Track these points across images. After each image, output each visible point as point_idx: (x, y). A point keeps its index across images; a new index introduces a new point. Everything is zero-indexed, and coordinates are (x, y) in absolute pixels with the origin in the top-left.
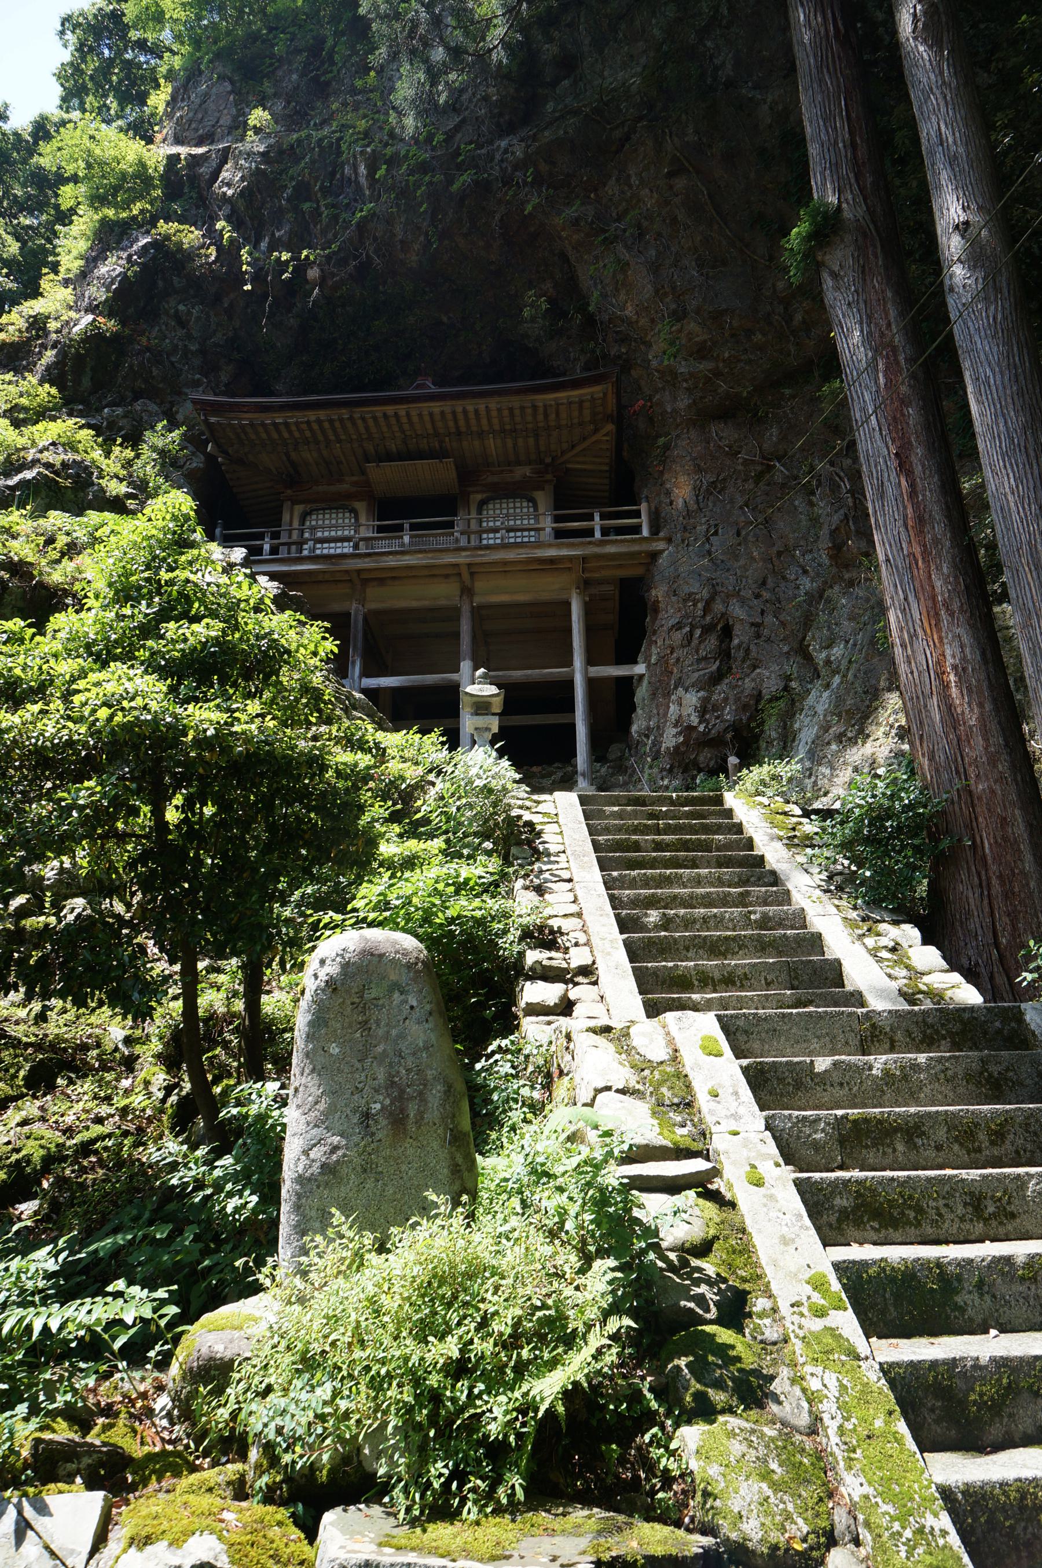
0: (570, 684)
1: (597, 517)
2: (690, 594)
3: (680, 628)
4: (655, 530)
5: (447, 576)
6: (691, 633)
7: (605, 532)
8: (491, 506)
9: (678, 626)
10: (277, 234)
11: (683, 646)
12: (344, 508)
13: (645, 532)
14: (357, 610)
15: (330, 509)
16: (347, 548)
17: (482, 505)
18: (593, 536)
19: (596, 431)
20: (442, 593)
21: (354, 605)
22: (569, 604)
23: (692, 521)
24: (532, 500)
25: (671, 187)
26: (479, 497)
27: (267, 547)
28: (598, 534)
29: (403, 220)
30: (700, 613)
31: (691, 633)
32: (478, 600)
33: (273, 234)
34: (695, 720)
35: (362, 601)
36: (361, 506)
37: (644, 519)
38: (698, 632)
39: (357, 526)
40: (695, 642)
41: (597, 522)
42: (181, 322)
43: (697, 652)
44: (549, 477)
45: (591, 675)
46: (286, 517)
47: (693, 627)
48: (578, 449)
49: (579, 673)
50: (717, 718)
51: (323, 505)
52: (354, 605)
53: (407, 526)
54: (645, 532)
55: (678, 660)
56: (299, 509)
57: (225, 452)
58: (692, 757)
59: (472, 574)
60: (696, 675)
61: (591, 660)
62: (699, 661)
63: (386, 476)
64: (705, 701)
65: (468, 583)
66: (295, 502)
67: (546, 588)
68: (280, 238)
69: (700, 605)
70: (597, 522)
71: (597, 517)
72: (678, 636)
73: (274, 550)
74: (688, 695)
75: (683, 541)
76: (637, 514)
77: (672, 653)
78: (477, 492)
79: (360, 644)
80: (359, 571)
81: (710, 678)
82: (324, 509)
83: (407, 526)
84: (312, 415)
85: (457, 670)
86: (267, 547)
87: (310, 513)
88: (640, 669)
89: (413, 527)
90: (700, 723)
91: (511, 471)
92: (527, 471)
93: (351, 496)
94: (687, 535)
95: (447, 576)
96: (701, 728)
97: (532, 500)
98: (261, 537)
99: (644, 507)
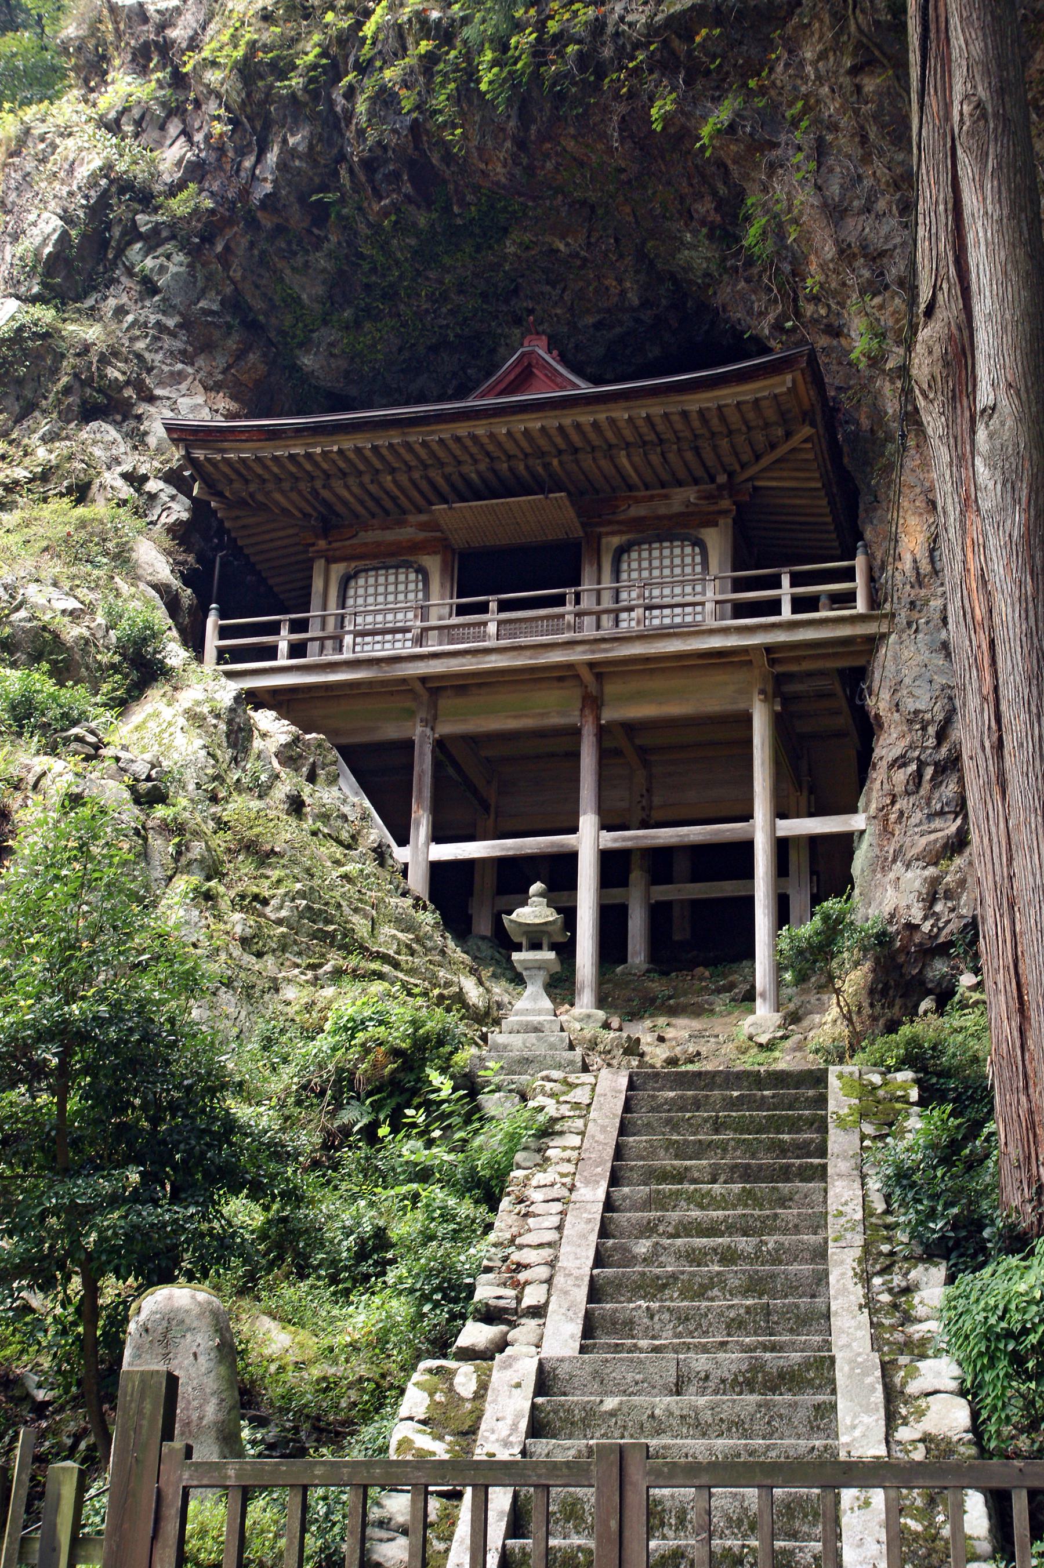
0: (747, 847)
1: (786, 580)
2: (917, 712)
3: (904, 765)
4: (874, 602)
5: (560, 679)
6: (919, 774)
7: (800, 604)
8: (634, 555)
9: (900, 762)
10: (291, 141)
11: (908, 793)
12: (407, 565)
13: (861, 606)
14: (423, 735)
15: (387, 568)
16: (403, 646)
17: (620, 552)
18: (779, 613)
19: (788, 435)
20: (554, 709)
21: (419, 729)
22: (747, 720)
23: (923, 592)
24: (699, 543)
25: (859, 88)
26: (616, 541)
27: (283, 647)
28: (786, 612)
29: (477, 118)
30: (931, 742)
31: (919, 774)
32: (608, 715)
33: (285, 141)
34: (916, 915)
35: (431, 722)
36: (433, 564)
37: (860, 584)
38: (929, 771)
39: (424, 612)
40: (926, 786)
41: (786, 591)
42: (149, 287)
43: (928, 804)
44: (726, 504)
45: (780, 833)
46: (318, 584)
47: (922, 765)
48: (765, 462)
49: (761, 830)
50: (952, 910)
51: (375, 563)
52: (419, 729)
53: (493, 606)
54: (861, 606)
55: (901, 813)
56: (338, 570)
57: (219, 494)
58: (915, 971)
59: (599, 677)
60: (923, 841)
61: (781, 812)
62: (931, 817)
63: (469, 520)
64: (934, 882)
65: (593, 688)
66: (330, 561)
67: (711, 698)
68: (294, 149)
69: (932, 730)
70: (786, 591)
71: (786, 580)
72: (901, 776)
73: (297, 650)
74: (910, 874)
75: (909, 624)
76: (849, 575)
77: (893, 803)
78: (613, 533)
79: (427, 793)
80: (424, 679)
81: (945, 846)
82: (377, 569)
83: (493, 606)
84: (348, 443)
85: (574, 830)
86: (283, 647)
87: (355, 576)
88: (857, 822)
89: (504, 606)
90: (925, 918)
91: (666, 497)
92: (691, 494)
93: (417, 547)
94: (915, 615)
95: (560, 679)
96: (926, 927)
97: (699, 543)
98: (273, 629)
99: (859, 563)
